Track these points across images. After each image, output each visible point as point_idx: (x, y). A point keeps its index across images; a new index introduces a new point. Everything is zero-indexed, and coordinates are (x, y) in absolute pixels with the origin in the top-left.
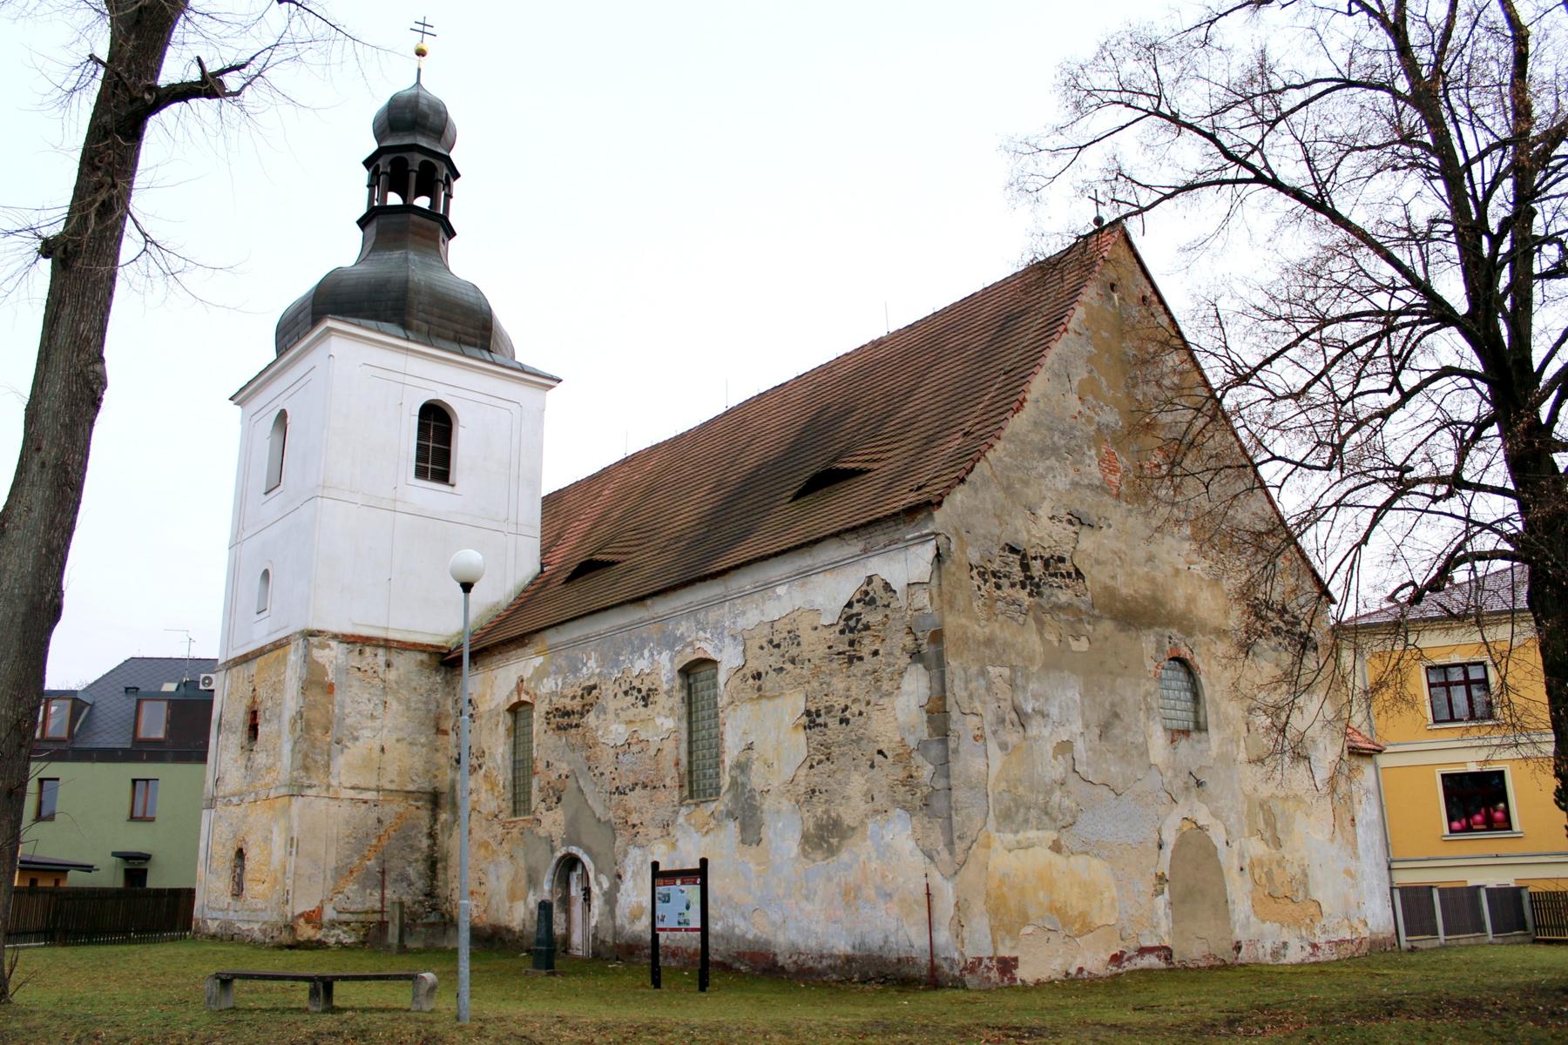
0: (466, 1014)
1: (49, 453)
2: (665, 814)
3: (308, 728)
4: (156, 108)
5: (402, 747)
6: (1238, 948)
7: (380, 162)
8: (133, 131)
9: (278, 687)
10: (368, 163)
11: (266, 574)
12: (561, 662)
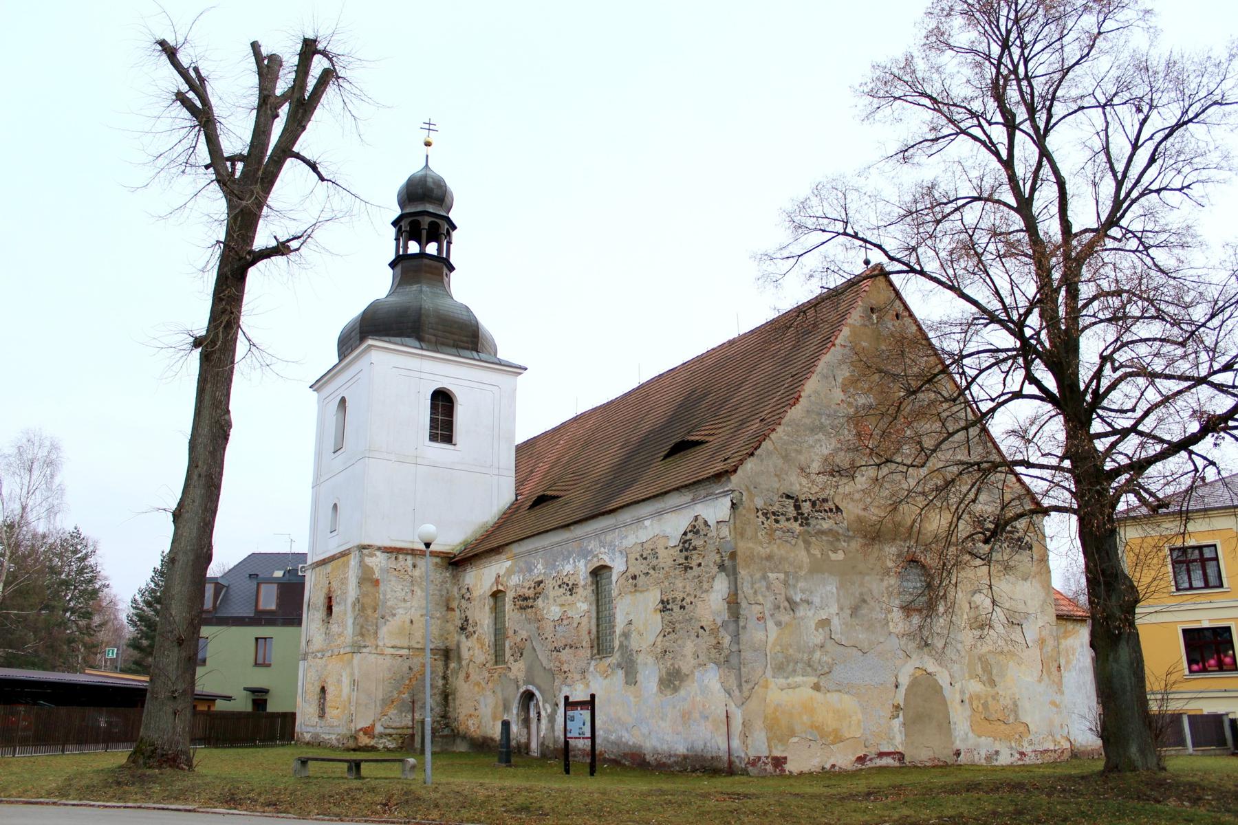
0: (429, 780)
1: (203, 468)
2: (583, 664)
3: (363, 609)
4: (253, 263)
6: (958, 753)
7: (402, 224)
8: (241, 277)
9: (344, 581)
10: (395, 224)
11: (335, 505)
12: (522, 564)
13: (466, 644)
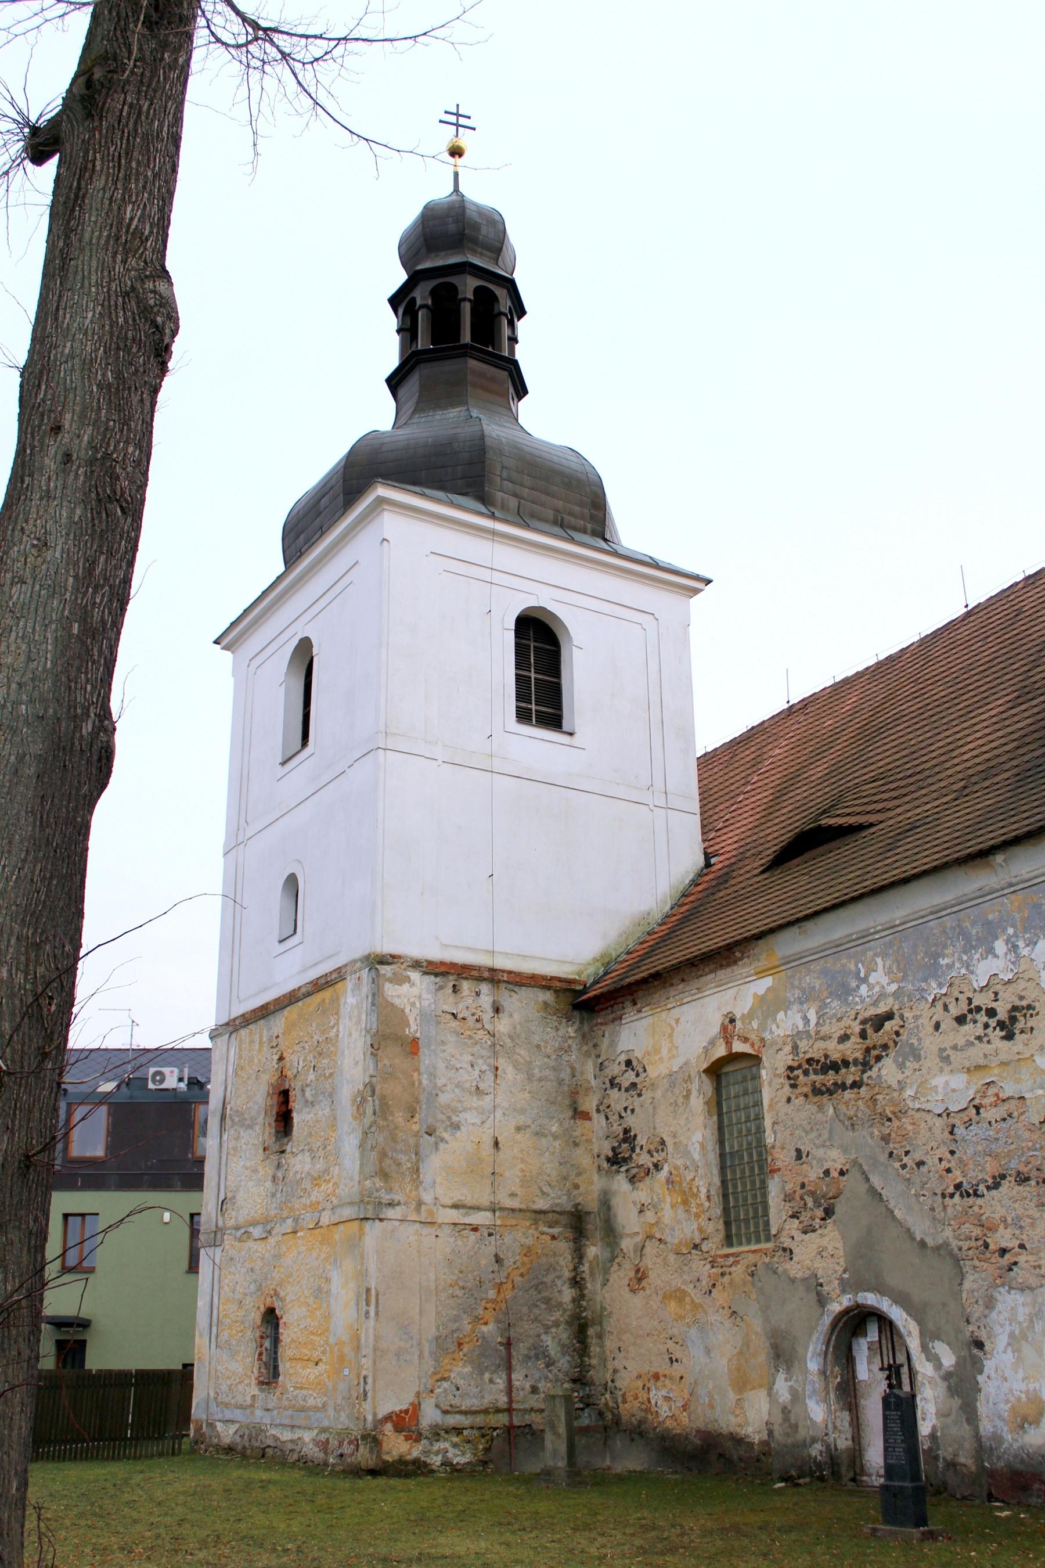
1: (76, 435)
3: (384, 1110)
5: (524, 1139)
9: (325, 1049)
10: (395, 301)
11: (292, 882)
13: (628, 1200)
